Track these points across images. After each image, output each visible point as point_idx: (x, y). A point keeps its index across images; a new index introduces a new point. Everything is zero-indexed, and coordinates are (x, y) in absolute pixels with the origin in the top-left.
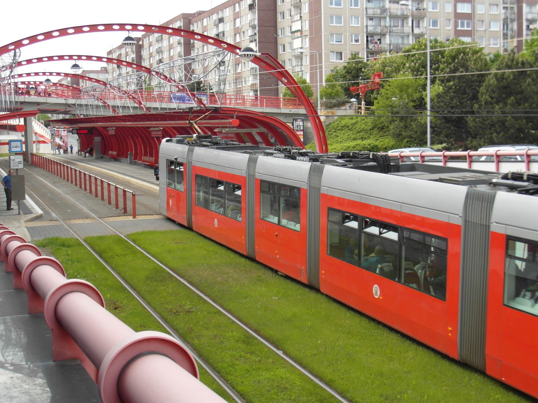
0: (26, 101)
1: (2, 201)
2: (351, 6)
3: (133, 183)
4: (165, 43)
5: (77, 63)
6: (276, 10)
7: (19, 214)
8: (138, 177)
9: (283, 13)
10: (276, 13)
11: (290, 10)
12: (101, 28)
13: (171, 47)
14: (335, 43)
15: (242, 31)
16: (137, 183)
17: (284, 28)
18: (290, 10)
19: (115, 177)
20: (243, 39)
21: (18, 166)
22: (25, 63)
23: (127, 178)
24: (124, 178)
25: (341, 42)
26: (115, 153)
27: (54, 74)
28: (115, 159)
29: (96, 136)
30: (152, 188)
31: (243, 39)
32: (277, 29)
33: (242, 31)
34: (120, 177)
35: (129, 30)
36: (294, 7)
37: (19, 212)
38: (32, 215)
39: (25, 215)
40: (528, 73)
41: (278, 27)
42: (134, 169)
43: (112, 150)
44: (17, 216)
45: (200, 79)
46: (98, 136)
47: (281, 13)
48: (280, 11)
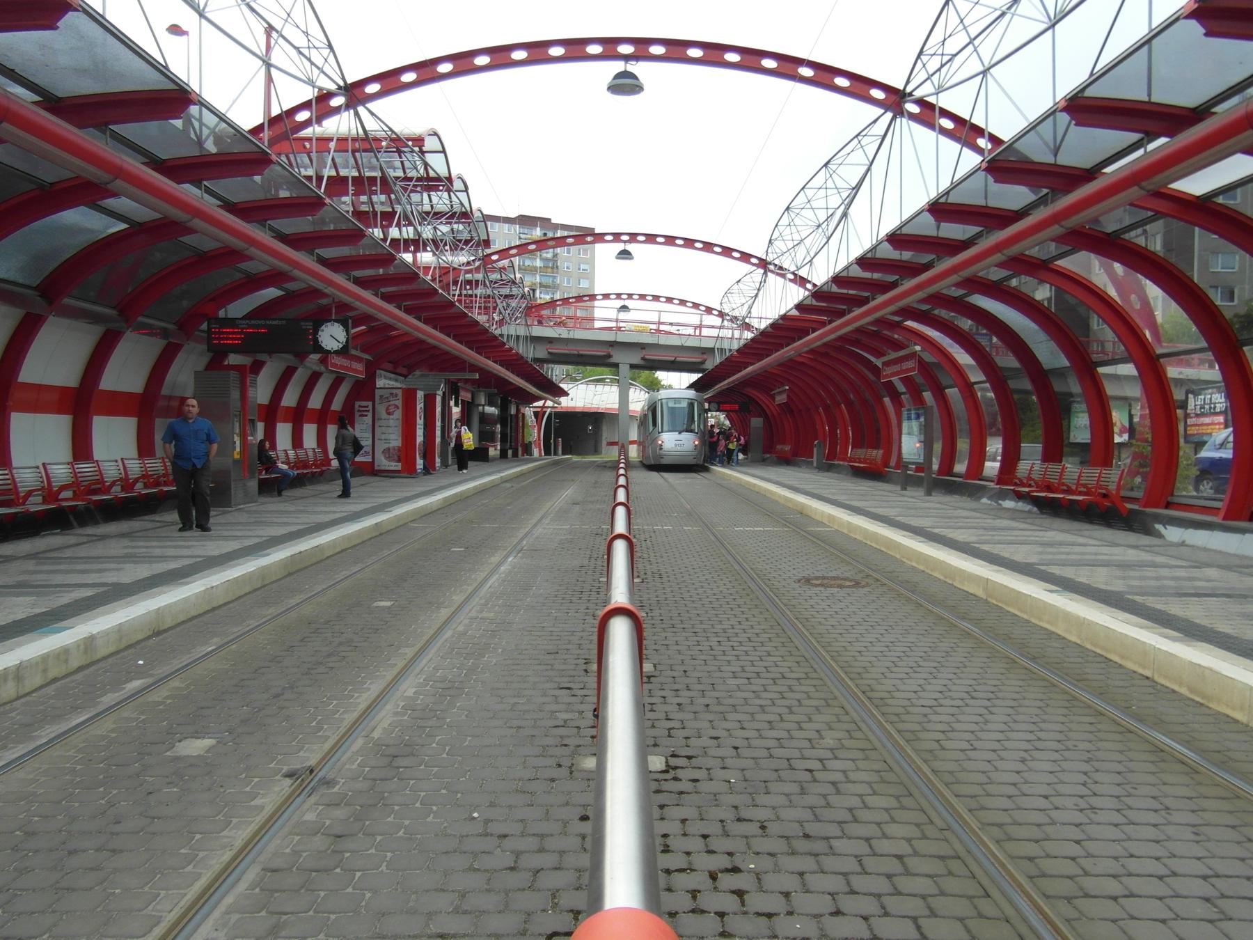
3: (818, 518)
8: (835, 497)
12: (718, 249)
14: (1219, 270)
16: (831, 517)
19: (768, 495)
22: (637, 297)
23: (801, 499)
24: (790, 500)
25: (1233, 268)
26: (787, 448)
27: (634, 297)
28: (786, 460)
29: (755, 416)
30: (898, 546)
34: (780, 496)
35: (625, 242)
42: (826, 480)
43: (784, 443)
45: (398, 225)
46: (760, 416)
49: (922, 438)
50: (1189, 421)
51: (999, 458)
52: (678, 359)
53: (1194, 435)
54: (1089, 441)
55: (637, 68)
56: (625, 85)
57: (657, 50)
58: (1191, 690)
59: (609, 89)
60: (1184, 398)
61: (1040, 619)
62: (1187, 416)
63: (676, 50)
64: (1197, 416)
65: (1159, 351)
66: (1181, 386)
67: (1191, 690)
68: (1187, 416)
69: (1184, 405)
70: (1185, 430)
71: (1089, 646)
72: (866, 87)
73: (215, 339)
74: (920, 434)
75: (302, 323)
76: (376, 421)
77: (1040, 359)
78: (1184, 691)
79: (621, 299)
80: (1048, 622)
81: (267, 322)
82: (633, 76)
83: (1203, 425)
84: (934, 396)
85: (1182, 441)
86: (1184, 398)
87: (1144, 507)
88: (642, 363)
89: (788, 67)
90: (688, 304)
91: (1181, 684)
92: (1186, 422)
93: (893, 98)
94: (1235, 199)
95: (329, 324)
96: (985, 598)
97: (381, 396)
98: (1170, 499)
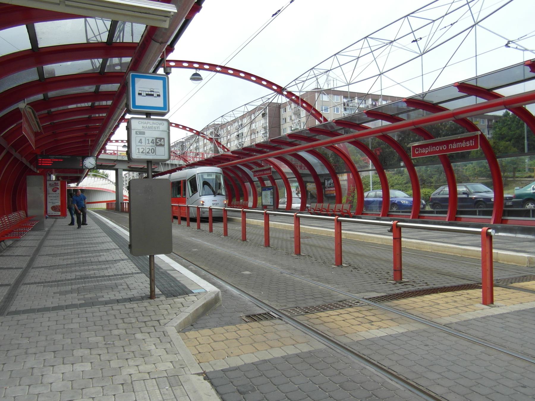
0: (118, 159)
1: (98, 248)
2: (334, 112)
4: (201, 143)
5: (198, 72)
6: (280, 118)
7: (152, 296)
9: (285, 119)
10: (280, 119)
11: (291, 117)
13: (205, 145)
15: (256, 131)
17: (286, 129)
18: (291, 117)
20: (257, 137)
21: (154, 151)
31: (257, 137)
32: (280, 130)
33: (256, 131)
36: (294, 114)
37: (152, 291)
38: (192, 298)
39: (170, 301)
40: (472, 152)
41: (281, 128)
44: (146, 303)
47: (283, 119)
48: (283, 118)
49: (272, 197)
50: (326, 189)
51: (286, 203)
52: (103, 164)
53: (327, 194)
54: (448, 196)
55: (201, 72)
56: (196, 77)
57: (206, 67)
58: (416, 248)
59: (190, 79)
60: (323, 181)
61: (368, 240)
62: (325, 188)
63: (213, 67)
64: (329, 187)
65: (358, 170)
66: (323, 177)
67: (416, 248)
68: (325, 188)
69: (324, 183)
70: (325, 192)
71: (385, 244)
72: (271, 85)
73: (40, 163)
74: (271, 195)
75: (77, 158)
76: (48, 194)
77: (316, 171)
78: (415, 248)
79: (123, 142)
80: (371, 241)
81: (63, 157)
82: (199, 75)
83: (331, 190)
84: (260, 183)
85: (324, 196)
86: (323, 181)
87: (357, 214)
88: (128, 168)
89: (269, 85)
90: (119, 141)
91: (414, 247)
92: (325, 190)
93: (279, 89)
94: (328, 112)
95: (88, 158)
96: (345, 238)
97: (50, 184)
98: (362, 212)
